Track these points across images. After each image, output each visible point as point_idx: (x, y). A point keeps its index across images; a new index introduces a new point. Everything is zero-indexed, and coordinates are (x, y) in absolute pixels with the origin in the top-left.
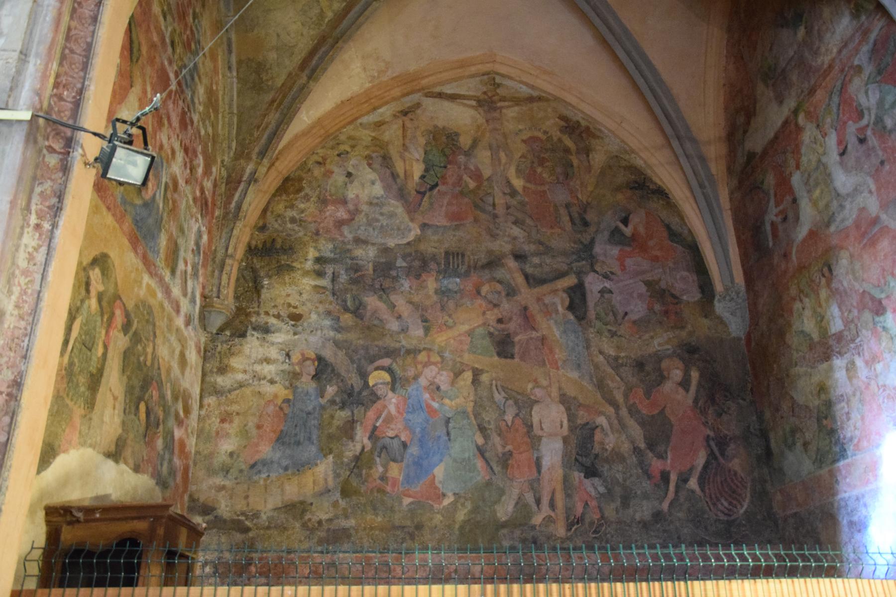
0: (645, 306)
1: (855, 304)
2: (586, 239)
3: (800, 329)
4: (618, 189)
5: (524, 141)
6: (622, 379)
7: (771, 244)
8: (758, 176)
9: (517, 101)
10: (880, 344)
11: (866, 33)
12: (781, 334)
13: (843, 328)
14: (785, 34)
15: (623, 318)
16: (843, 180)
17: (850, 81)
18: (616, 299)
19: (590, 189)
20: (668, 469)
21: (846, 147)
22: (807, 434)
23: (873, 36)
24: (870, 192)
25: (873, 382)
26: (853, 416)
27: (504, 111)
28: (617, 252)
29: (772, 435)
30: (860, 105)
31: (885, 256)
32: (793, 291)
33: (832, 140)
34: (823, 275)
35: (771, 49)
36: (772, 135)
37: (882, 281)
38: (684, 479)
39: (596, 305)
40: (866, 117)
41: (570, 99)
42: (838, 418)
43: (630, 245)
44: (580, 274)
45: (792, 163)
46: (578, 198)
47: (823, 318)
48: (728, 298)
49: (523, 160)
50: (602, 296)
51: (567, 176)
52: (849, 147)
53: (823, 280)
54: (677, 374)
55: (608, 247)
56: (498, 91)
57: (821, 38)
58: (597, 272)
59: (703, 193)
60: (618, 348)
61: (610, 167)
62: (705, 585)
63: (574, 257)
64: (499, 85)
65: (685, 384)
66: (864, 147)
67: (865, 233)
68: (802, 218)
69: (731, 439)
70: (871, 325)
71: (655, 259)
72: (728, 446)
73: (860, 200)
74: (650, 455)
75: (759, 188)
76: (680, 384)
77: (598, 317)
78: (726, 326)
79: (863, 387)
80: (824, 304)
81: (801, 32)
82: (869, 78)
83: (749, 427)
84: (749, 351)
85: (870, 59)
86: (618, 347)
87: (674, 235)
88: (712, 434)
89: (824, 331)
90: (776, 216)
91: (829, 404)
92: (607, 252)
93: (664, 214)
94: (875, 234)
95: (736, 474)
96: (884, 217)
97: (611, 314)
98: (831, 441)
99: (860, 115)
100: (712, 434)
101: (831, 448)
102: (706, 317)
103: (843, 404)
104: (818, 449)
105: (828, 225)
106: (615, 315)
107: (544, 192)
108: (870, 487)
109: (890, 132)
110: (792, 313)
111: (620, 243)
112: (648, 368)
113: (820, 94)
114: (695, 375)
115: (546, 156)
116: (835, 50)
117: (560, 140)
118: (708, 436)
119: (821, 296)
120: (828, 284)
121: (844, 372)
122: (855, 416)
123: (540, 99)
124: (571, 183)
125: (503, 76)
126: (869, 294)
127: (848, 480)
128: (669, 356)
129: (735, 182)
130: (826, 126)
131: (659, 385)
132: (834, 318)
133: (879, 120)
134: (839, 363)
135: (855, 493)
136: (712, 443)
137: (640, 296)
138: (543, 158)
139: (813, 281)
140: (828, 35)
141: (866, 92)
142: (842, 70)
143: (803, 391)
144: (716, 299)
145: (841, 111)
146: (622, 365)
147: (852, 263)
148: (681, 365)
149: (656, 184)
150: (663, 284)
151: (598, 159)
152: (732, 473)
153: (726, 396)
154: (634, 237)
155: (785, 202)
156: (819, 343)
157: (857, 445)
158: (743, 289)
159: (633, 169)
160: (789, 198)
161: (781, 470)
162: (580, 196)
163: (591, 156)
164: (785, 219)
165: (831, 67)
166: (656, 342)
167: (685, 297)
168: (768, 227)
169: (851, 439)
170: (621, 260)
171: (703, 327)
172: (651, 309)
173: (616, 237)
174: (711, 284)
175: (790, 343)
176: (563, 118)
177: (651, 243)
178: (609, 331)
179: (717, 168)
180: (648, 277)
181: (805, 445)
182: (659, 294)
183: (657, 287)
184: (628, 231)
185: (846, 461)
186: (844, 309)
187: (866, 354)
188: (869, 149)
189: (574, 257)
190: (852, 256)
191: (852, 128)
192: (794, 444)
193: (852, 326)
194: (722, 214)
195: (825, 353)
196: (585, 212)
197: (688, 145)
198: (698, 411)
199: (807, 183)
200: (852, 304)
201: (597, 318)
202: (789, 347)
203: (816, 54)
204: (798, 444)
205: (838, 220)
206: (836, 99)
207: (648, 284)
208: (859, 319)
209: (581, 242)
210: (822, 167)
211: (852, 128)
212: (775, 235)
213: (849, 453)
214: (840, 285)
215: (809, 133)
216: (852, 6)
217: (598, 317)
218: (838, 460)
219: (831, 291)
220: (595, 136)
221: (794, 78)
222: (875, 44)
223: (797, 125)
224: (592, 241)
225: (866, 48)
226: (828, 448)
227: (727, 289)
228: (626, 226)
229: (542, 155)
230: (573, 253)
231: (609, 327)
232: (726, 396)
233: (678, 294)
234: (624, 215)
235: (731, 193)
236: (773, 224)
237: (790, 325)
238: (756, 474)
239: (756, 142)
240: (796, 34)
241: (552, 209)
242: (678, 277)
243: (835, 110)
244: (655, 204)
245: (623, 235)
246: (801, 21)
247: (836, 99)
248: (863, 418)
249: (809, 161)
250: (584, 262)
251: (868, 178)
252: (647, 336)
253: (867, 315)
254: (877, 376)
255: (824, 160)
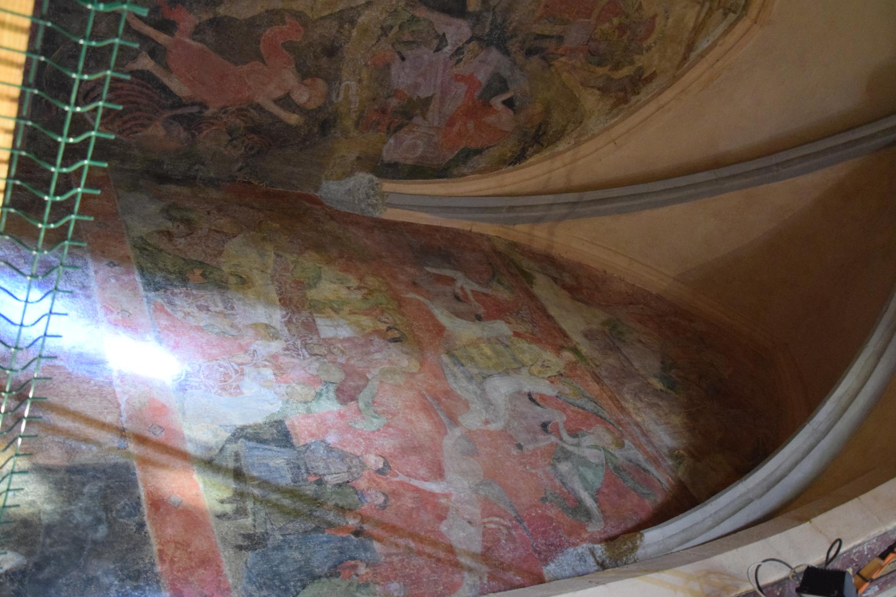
0: (402, 87)
1: (352, 362)
2: (513, 46)
3: (323, 276)
4: (547, 111)
5: (656, 15)
6: (322, 18)
7: (429, 269)
8: (508, 278)
9: (698, 29)
10: (299, 384)
11: (655, 461)
12: (318, 247)
13: (322, 336)
14: (654, 364)
15: (399, 53)
16: (501, 388)
17: (608, 430)
18: (426, 54)
19: (565, 75)
20: (177, 35)
21: (538, 405)
22: (182, 240)
23: (652, 469)
24: (487, 422)
25: (248, 358)
26: (203, 315)
27: (698, 7)
28: (480, 78)
29: (186, 190)
30: (583, 435)
31: (411, 422)
32: (371, 281)
33: (544, 388)
34: (389, 329)
35: (640, 341)
36: (552, 313)
37: (380, 409)
38: (155, 52)
39: (431, 23)
40: (570, 440)
41: (669, 94)
42: (202, 293)
43: (480, 98)
44: (477, 18)
45: (521, 329)
46: (562, 55)
47: (336, 311)
48: (372, 192)
49: (636, 6)
50: (438, 36)
51: (592, 53)
52: (539, 408)
53: (383, 327)
54: (302, 96)
55: (491, 69)
56: (721, 10)
57: (651, 405)
58: (468, 42)
59: (502, 207)
60: (365, 31)
61: (574, 110)
62: (17, 29)
63: (499, 20)
64: (726, 15)
65: (286, 102)
66: (538, 428)
67: (440, 403)
68: (458, 321)
69: (193, 136)
70: (324, 377)
71: (451, 123)
72: (185, 129)
73: (477, 405)
74: (205, 17)
75: (494, 275)
76: (288, 95)
77: (413, 19)
78: (339, 179)
79: (243, 343)
80: (353, 318)
81: (659, 386)
82: (612, 454)
83: (203, 164)
84: (300, 196)
85: (630, 461)
86: (366, 30)
87: (467, 155)
88: (208, 113)
89: (317, 307)
90: (462, 288)
91: (221, 285)
92: (486, 64)
93: (495, 152)
94: (437, 415)
95: (144, 126)
96: (457, 432)
97: (411, 39)
98: (171, 273)
99: (574, 434)
100: (208, 113)
101: (161, 270)
102: (358, 158)
103: (221, 307)
104: (161, 250)
105: (449, 353)
106: (408, 43)
107: (589, 16)
108: (101, 313)
109: (554, 466)
110: (345, 271)
111: (489, 86)
112: (324, 61)
113: (595, 387)
114: (293, 119)
115: (625, 37)
116: (639, 419)
117: (632, 63)
118: (206, 108)
119: (364, 318)
120: (377, 332)
121: (264, 320)
122: (203, 319)
123: (685, 58)
124: (581, 55)
125: (732, 26)
126: (365, 386)
127: (113, 281)
128: (328, 95)
129: (501, 247)
130: (561, 386)
131: (297, 66)
132: (336, 327)
133: (567, 456)
134: (277, 317)
135: (94, 285)
136: (195, 109)
137: (416, 86)
138: (625, 33)
139: (383, 312)
140: (653, 415)
141: (596, 447)
142: (619, 423)
143: (240, 254)
144: (375, 179)
145: (576, 409)
146: (341, 27)
147: (404, 372)
148: (312, 106)
149: (531, 156)
150: (418, 120)
151: (590, 100)
152: (146, 122)
153: (252, 148)
154: (486, 106)
155: (476, 303)
156: (305, 295)
157: (162, 310)
158: (377, 215)
159: (560, 135)
160: (482, 311)
161: (135, 187)
162: (563, 59)
163: (597, 92)
164: (457, 298)
165: (622, 409)
166: (353, 84)
167: (392, 141)
168: (448, 273)
169: (171, 303)
170: (469, 80)
171: (347, 150)
172: (396, 93)
173: (499, 84)
174: (394, 178)
175: (306, 255)
176: (653, 76)
177: (471, 125)
178: (392, 27)
179: (520, 232)
180: (434, 106)
181: (169, 235)
182: (410, 111)
183: (418, 111)
184: (497, 102)
185: (141, 287)
186: (347, 345)
187: (287, 360)
188: (535, 433)
189: (499, 20)
190: (412, 375)
191: (559, 418)
192: (172, 219)
193: (323, 351)
194: (468, 219)
195: (291, 300)
196: (544, 58)
197: (564, 210)
198: (244, 106)
199: (498, 340)
200: (353, 357)
201: (413, 17)
202: (301, 253)
203: (635, 394)
204: (170, 224)
205: (455, 369)
206: (590, 406)
207: (427, 101)
208: (333, 362)
209: (512, 37)
210: (516, 366)
211: (559, 418)
212: (439, 279)
213: (152, 294)
214: (376, 348)
215: (556, 362)
216: (682, 452)
217: (413, 19)
218: (143, 275)
219: (370, 334)
220: (615, 106)
221: (611, 361)
222: (645, 470)
223: (562, 348)
224: (506, 52)
225: (641, 457)
226: (161, 265)
227: (383, 195)
228: (504, 102)
229: (628, 33)
230: (504, 21)
231: (396, 29)
232: (252, 148)
233: (401, 134)
234: (517, 104)
235: (489, 239)
236: (453, 280)
237: (329, 262)
238: (136, 152)
239: (543, 288)
240: (655, 376)
241: (567, 16)
242: (419, 142)
243: (578, 402)
244: (509, 147)
245: (496, 94)
246: (669, 387)
247: (590, 406)
248: (199, 329)
249: (523, 352)
250: (487, 30)
251: (503, 423)
252: (365, 75)
253: (337, 376)
254: (256, 366)
255: (524, 371)
